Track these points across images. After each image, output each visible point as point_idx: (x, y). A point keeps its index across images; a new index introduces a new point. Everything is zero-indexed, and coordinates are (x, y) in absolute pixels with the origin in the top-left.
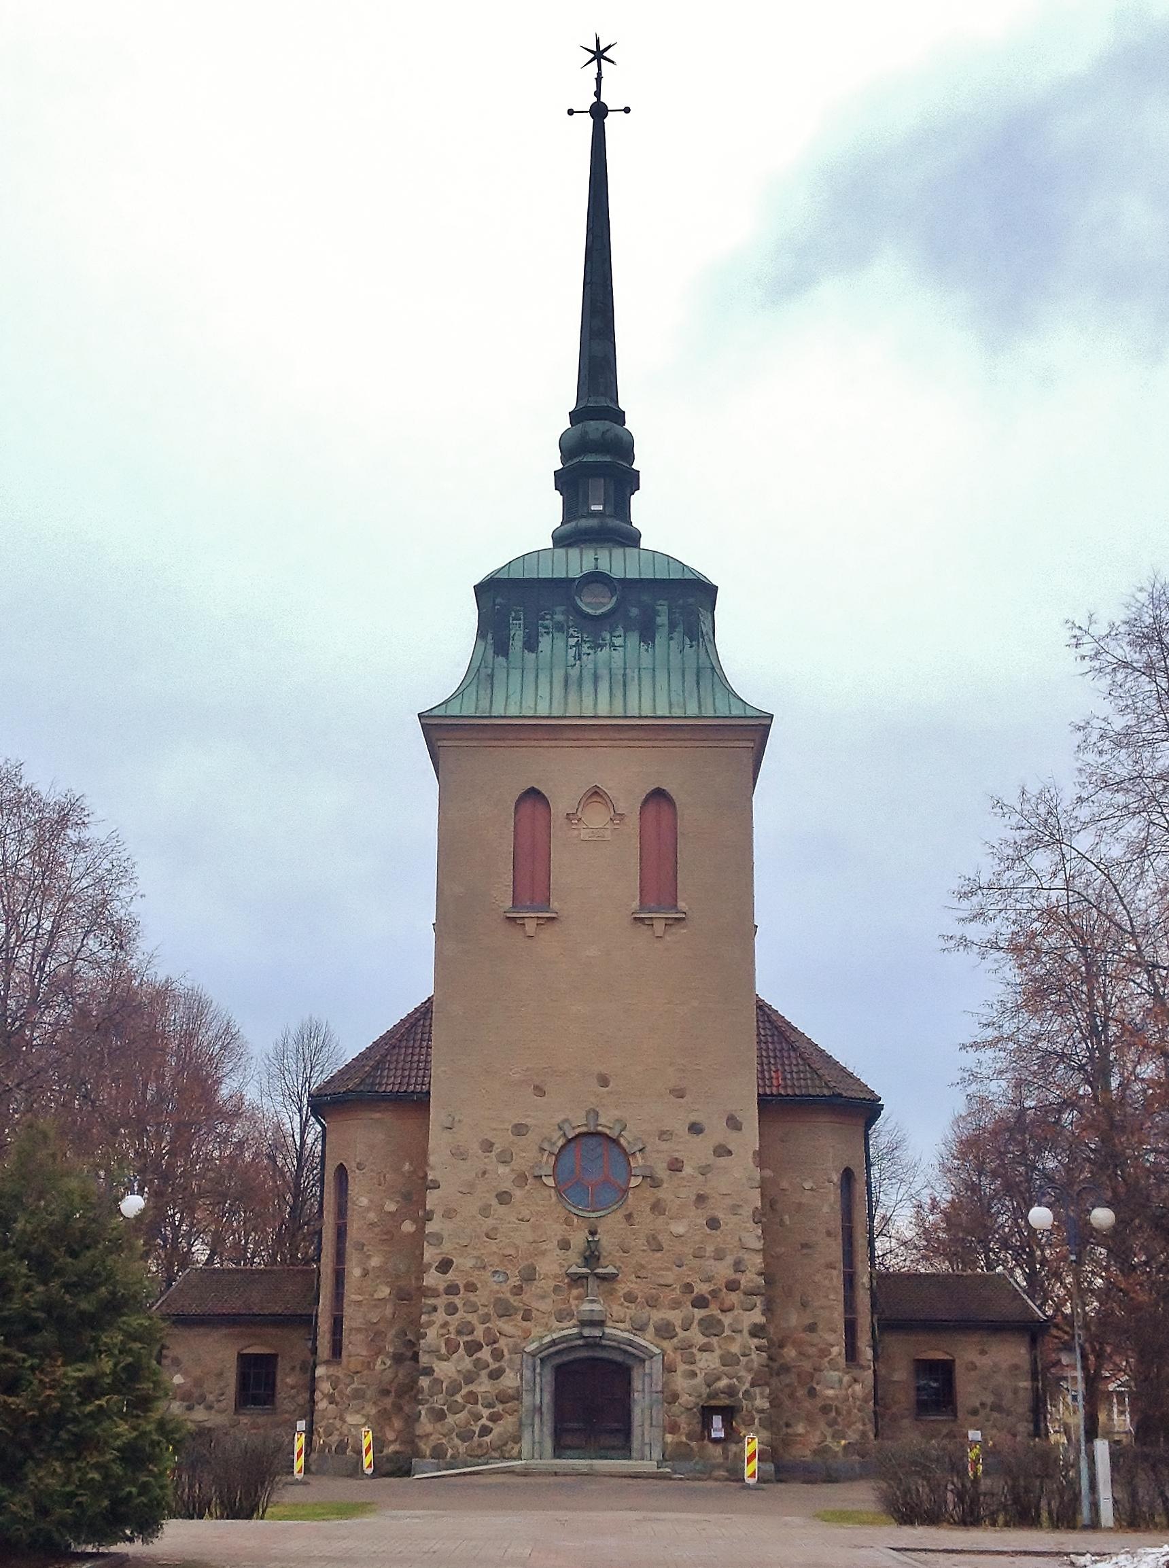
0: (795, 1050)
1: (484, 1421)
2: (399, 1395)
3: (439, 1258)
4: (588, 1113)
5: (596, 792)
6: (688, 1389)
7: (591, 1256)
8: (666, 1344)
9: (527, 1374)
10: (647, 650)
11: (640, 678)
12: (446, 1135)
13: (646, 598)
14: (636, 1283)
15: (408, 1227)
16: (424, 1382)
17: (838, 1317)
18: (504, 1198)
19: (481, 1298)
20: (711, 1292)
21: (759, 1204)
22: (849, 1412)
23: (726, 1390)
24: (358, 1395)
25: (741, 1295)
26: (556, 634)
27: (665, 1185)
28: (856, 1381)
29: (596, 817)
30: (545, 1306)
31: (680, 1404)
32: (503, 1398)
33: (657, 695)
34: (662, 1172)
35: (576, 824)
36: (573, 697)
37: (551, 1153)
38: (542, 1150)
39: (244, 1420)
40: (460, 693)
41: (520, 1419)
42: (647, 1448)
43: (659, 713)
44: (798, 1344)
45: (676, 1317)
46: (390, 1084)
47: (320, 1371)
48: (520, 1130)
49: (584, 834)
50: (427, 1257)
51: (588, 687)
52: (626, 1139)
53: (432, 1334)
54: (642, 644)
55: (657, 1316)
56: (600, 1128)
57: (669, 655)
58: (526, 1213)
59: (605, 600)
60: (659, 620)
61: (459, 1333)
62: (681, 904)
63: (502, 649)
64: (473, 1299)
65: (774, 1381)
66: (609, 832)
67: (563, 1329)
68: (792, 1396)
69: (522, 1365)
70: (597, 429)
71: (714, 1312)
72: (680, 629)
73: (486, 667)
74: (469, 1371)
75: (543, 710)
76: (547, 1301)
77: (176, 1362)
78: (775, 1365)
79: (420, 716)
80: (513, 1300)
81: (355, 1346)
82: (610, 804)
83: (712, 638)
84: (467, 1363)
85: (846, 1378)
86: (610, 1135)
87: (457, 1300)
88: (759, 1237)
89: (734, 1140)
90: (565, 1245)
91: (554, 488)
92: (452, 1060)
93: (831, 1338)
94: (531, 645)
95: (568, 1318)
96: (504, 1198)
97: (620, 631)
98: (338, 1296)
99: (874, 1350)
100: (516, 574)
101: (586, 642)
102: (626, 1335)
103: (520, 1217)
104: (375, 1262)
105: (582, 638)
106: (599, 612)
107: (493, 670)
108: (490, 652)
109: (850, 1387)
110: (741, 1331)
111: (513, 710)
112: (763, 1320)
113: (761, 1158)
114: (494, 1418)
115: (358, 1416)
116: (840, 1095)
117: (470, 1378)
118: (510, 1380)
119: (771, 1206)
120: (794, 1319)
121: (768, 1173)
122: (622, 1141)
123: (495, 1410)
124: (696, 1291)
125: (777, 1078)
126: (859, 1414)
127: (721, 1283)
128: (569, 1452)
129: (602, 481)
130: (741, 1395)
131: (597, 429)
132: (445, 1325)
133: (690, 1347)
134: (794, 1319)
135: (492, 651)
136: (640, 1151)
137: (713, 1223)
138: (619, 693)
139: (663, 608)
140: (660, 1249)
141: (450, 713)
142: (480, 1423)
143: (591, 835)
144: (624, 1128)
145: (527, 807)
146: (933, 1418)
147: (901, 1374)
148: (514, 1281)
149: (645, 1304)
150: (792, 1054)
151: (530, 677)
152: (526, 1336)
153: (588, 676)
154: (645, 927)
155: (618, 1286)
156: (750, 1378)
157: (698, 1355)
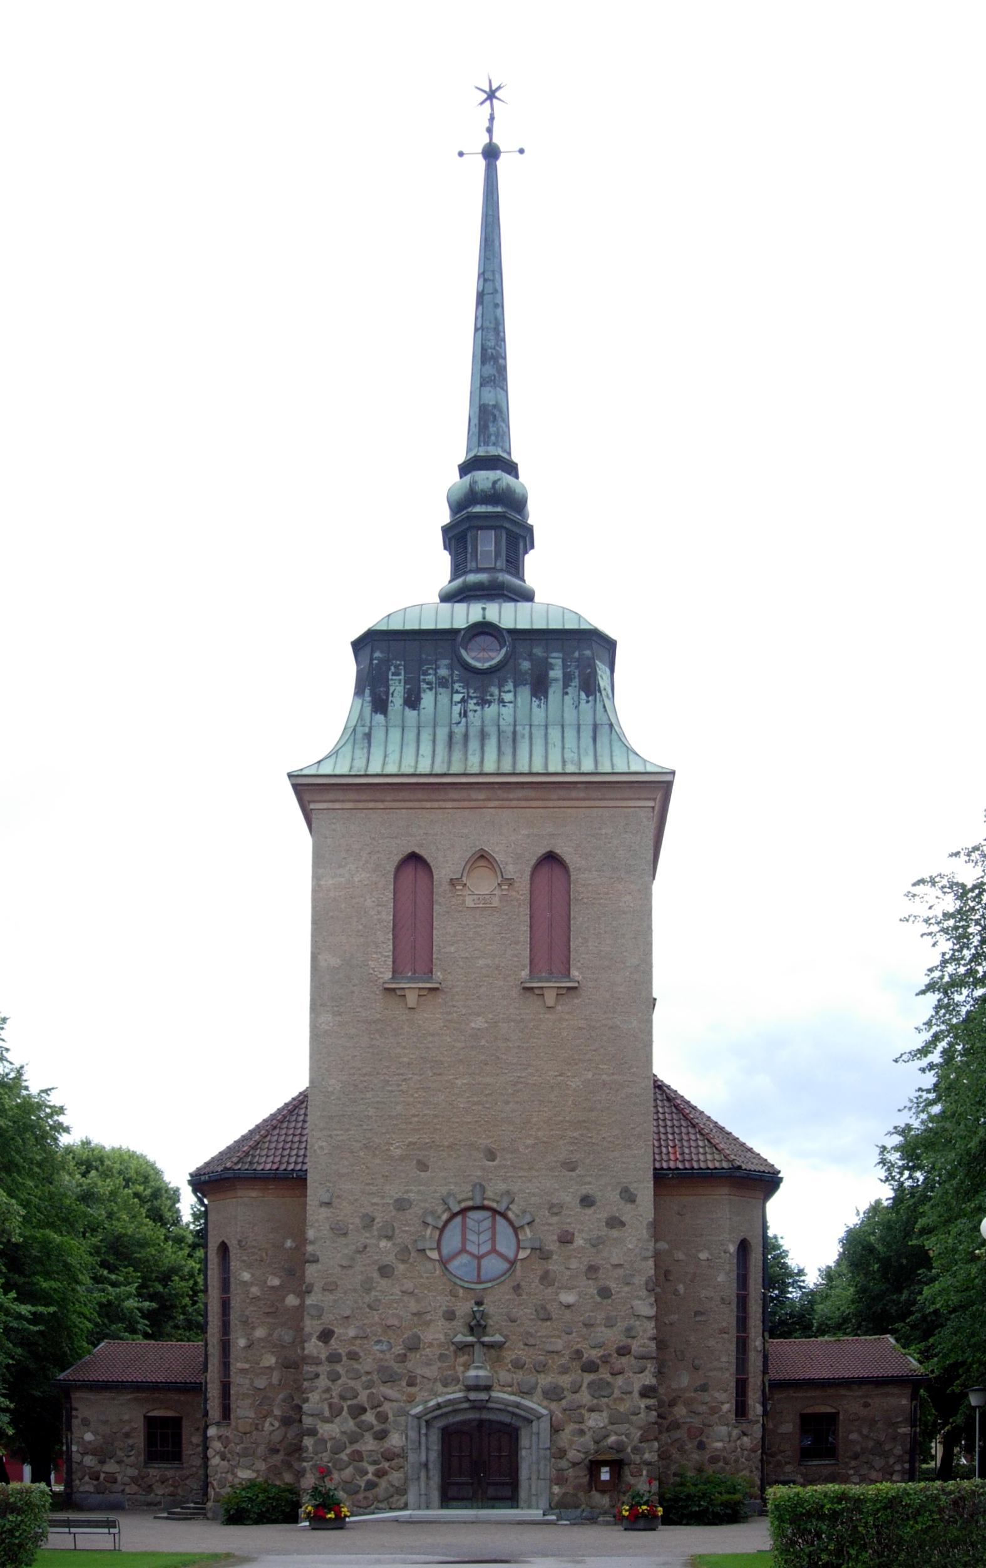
0: (694, 1126)
1: (370, 1476)
2: (288, 1454)
3: (320, 1328)
4: (474, 1186)
5: (482, 856)
6: (577, 1447)
7: (477, 1326)
8: (553, 1406)
9: (413, 1434)
10: (539, 706)
11: (531, 738)
12: (324, 1212)
13: (538, 651)
14: (523, 1350)
15: (292, 1300)
16: (308, 1442)
17: (729, 1377)
18: (385, 1271)
19: (367, 1364)
20: (601, 1357)
21: (652, 1272)
22: (736, 1461)
23: (614, 1446)
24: (245, 1454)
25: (633, 1359)
26: (441, 690)
27: (555, 1257)
28: (745, 1434)
29: (483, 885)
30: (431, 1372)
31: (568, 1460)
32: (389, 1456)
33: (550, 751)
34: (551, 1243)
35: (461, 890)
36: (457, 755)
37: (435, 1227)
38: (426, 1224)
39: (152, 1472)
40: (335, 753)
41: (406, 1473)
42: (534, 1498)
43: (551, 769)
44: (688, 1403)
45: (565, 1381)
46: (266, 1163)
47: (212, 1431)
48: (402, 1205)
49: (469, 902)
50: (307, 1330)
51: (474, 744)
52: (513, 1212)
53: (314, 1397)
54: (534, 699)
55: (545, 1380)
56: (486, 1203)
57: (563, 711)
58: (409, 1285)
59: (492, 654)
60: (552, 674)
61: (343, 1398)
62: (575, 973)
63: (380, 705)
64: (356, 1366)
65: (664, 1437)
66: (497, 899)
67: (449, 1394)
68: (681, 1449)
69: (406, 1426)
70: (488, 478)
71: (603, 1376)
72: (575, 683)
73: (363, 726)
74: (353, 1432)
75: (424, 767)
76: (432, 1367)
77: (86, 1423)
78: (666, 1423)
79: (290, 776)
80: (396, 1367)
81: (243, 1410)
82: (497, 869)
83: (611, 696)
84: (351, 1425)
85: (735, 1432)
86: (498, 1209)
87: (339, 1368)
88: (651, 1305)
89: (627, 1212)
90: (450, 1316)
91: (442, 547)
92: (330, 1136)
93: (721, 1396)
94: (412, 701)
95: (454, 1383)
96: (385, 1271)
97: (510, 686)
98: (226, 1365)
99: (764, 1405)
100: (396, 625)
101: (472, 698)
102: (513, 1398)
103: (404, 1289)
104: (260, 1333)
105: (468, 693)
106: (487, 665)
107: (370, 728)
108: (368, 709)
109: (739, 1438)
110: (630, 1393)
111: (391, 769)
112: (654, 1381)
113: (657, 1229)
114: (381, 1474)
115: (249, 1472)
116: (739, 1167)
117: (354, 1439)
118: (395, 1440)
119: (665, 1276)
120: (684, 1380)
121: (663, 1245)
122: (510, 1214)
123: (381, 1466)
124: (586, 1355)
125: (675, 1153)
126: (747, 1463)
127: (612, 1349)
128: (455, 1504)
129: (493, 532)
130: (629, 1450)
131: (488, 478)
132: (328, 1390)
133: (579, 1407)
134: (684, 1380)
135: (370, 708)
136: (528, 1224)
137: (605, 1293)
138: (507, 749)
139: (556, 660)
140: (549, 1319)
141: (322, 771)
142: (366, 1478)
143: (476, 901)
144: (512, 1202)
145: (409, 872)
146: (815, 1463)
147: (788, 1427)
148: (399, 1350)
149: (533, 1370)
150: (690, 1129)
151: (411, 736)
152: (411, 1400)
153: (473, 732)
154: (535, 997)
155: (504, 1353)
156: (639, 1434)
157: (587, 1415)
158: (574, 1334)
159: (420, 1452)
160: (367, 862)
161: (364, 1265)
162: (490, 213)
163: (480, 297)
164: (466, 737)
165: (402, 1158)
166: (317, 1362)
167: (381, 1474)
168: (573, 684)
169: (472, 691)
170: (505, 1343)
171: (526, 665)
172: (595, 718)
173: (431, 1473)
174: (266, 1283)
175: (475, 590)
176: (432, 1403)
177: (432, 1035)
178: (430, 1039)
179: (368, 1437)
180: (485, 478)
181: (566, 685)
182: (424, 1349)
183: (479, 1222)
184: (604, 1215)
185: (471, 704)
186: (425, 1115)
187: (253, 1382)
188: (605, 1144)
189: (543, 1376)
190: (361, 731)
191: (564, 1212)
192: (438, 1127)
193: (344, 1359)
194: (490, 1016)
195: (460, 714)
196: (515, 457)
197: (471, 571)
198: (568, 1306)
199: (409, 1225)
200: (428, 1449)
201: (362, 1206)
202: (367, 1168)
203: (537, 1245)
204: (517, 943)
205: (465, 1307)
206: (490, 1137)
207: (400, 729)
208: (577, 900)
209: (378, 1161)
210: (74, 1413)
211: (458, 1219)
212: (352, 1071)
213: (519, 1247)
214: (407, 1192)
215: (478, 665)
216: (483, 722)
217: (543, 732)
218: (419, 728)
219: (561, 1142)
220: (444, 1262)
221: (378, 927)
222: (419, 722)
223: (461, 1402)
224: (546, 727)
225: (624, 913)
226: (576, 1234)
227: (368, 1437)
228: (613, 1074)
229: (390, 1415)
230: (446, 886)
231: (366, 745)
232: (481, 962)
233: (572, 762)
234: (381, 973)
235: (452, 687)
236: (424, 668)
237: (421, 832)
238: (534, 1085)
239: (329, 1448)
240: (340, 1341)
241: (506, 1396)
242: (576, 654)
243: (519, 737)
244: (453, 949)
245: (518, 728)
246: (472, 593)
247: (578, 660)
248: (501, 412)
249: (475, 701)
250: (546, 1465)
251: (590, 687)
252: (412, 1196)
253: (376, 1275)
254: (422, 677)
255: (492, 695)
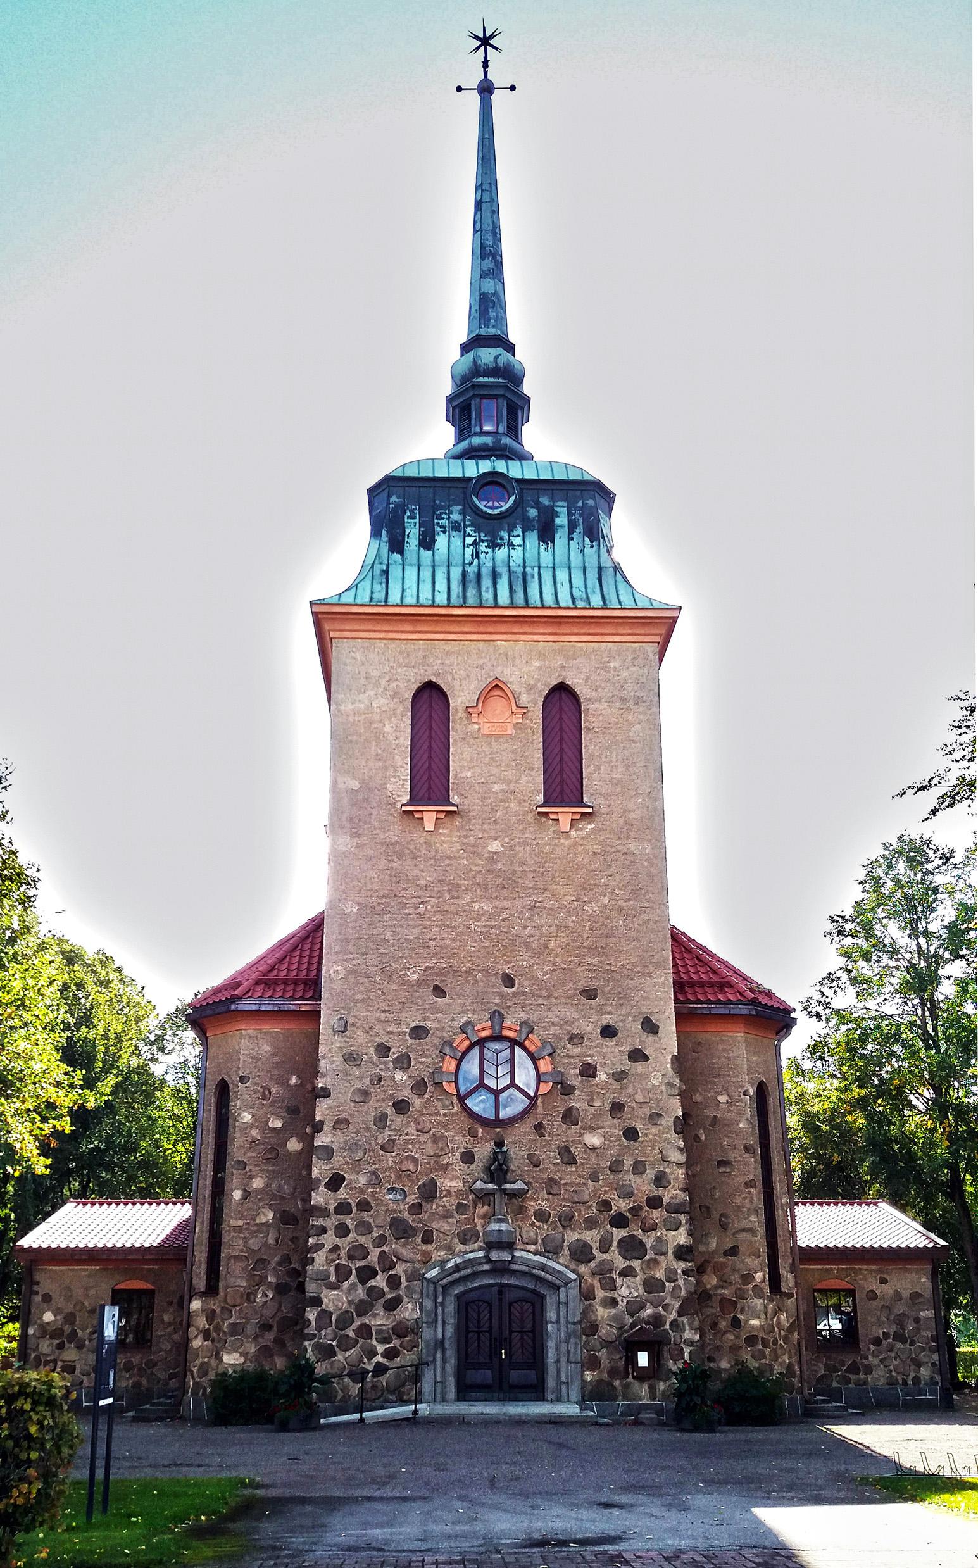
1: (379, 1358)
5: (497, 686)
7: (498, 1169)
8: (583, 1269)
10: (546, 550)
14: (547, 1200)
16: (311, 1315)
18: (401, 1106)
20: (631, 1210)
26: (454, 533)
27: (577, 1092)
32: (400, 1330)
40: (354, 586)
42: (564, 1388)
45: (591, 1237)
48: (419, 1033)
53: (320, 1258)
54: (541, 543)
55: (572, 1236)
61: (351, 1257)
63: (397, 545)
69: (422, 1294)
72: (580, 529)
73: (381, 563)
76: (450, 1220)
81: (235, 1278)
92: (346, 960)
94: (427, 542)
95: (474, 1239)
96: (401, 1106)
97: (519, 531)
101: (483, 541)
102: (537, 1258)
103: (420, 1127)
104: (257, 1183)
106: (496, 511)
107: (388, 566)
108: (385, 549)
112: (690, 1242)
118: (409, 1311)
132: (335, 1249)
137: (631, 1134)
139: (562, 509)
141: (344, 600)
158: (601, 1183)
159: (436, 1327)
160: (385, 689)
161: (378, 1101)
162: (486, 136)
163: (478, 205)
164: (479, 576)
165: (419, 984)
166: (324, 1212)
167: (390, 1354)
168: (577, 530)
169: (483, 535)
170: (528, 1190)
171: (533, 512)
172: (599, 562)
173: (449, 1353)
174: (268, 1124)
175: (479, 451)
176: (450, 1264)
177: (450, 858)
178: (447, 862)
179: (379, 1309)
180: (487, 356)
181: (571, 531)
182: (441, 1198)
183: (497, 1052)
184: (627, 1048)
185: (483, 547)
186: (443, 939)
187: (246, 1242)
188: (625, 971)
189: (569, 1232)
190: (378, 568)
191: (586, 1043)
192: (456, 951)
193: (354, 1209)
194: (507, 840)
195: (472, 555)
196: (512, 339)
197: (476, 434)
198: (594, 1149)
199: (426, 1057)
200: (444, 1323)
201: (377, 1035)
202: (383, 993)
203: (559, 1079)
204: (531, 769)
205: (484, 1150)
206: (508, 963)
207: (416, 568)
208: (588, 729)
209: (394, 987)
210: (35, 1288)
211: (476, 1051)
212: (369, 893)
213: (539, 1081)
214: (425, 1019)
215: (490, 511)
216: (494, 563)
217: (551, 573)
218: (434, 567)
219: (579, 969)
220: (461, 1099)
221: (396, 751)
222: (434, 561)
223: (482, 1263)
224: (554, 568)
225: (634, 742)
226: (599, 1068)
227: (379, 1309)
228: (629, 900)
229: (403, 1279)
230: (461, 714)
231: (384, 580)
232: (496, 788)
233: (581, 599)
234: (399, 796)
235: (465, 531)
236: (438, 513)
237: (439, 662)
238: (551, 909)
239: (334, 1321)
240: (351, 1189)
241: (530, 1256)
242: (580, 504)
243: (529, 577)
244: (469, 774)
245: (528, 569)
246: (477, 454)
247: (581, 509)
248: (499, 300)
249: (486, 544)
250: (576, 1344)
251: (594, 533)
252: (429, 1024)
253: (390, 1111)
254: (436, 521)
255: (502, 539)
